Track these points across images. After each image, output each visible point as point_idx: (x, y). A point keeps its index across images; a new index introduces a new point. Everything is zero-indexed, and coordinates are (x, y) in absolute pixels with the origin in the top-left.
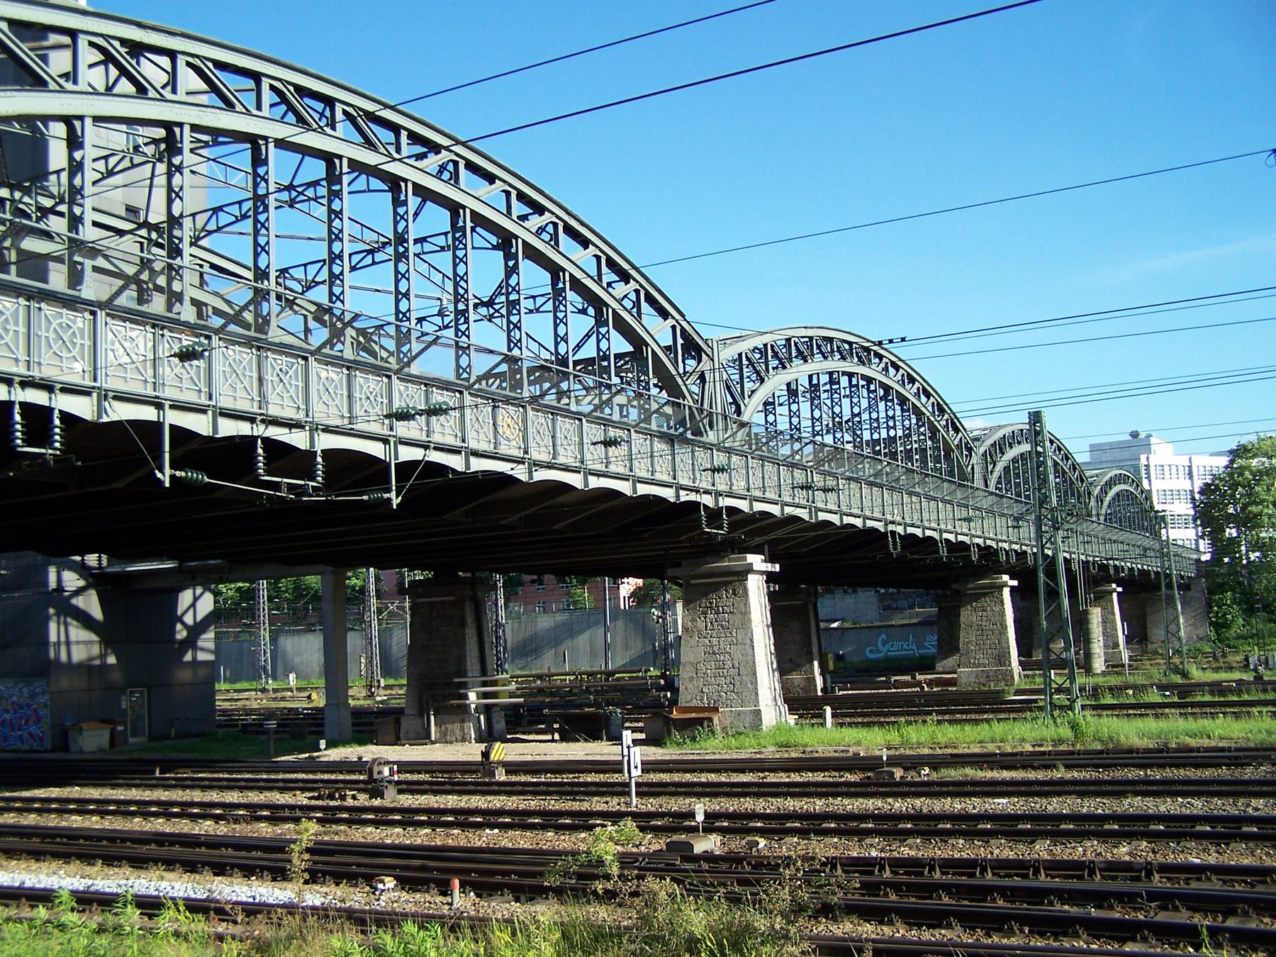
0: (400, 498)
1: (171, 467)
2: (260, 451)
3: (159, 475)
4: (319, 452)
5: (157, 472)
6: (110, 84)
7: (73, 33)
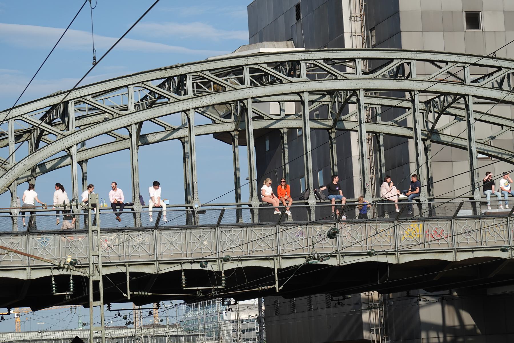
0: (281, 287)
1: (130, 291)
2: (183, 277)
3: (125, 295)
4: (223, 271)
5: (124, 294)
6: (497, 69)
7: (354, 60)
